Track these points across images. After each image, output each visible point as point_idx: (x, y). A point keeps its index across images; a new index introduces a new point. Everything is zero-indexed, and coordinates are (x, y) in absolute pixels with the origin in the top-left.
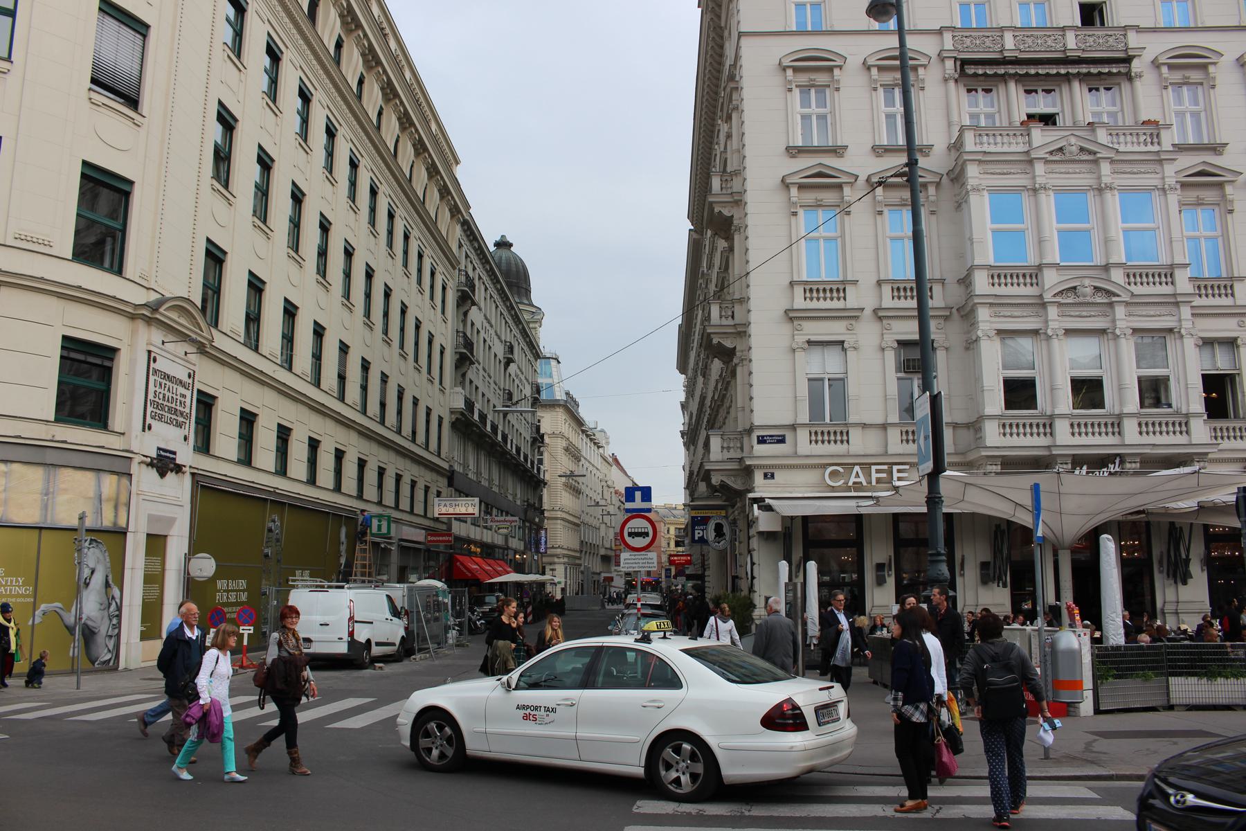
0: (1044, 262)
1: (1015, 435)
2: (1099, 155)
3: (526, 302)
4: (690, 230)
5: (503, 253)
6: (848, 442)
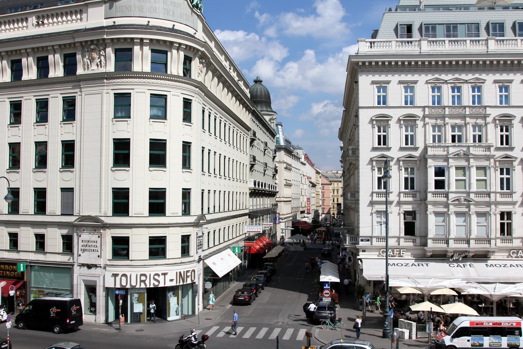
0: (450, 191)
1: (437, 244)
2: (470, 156)
3: (269, 110)
4: (344, 111)
5: (258, 86)
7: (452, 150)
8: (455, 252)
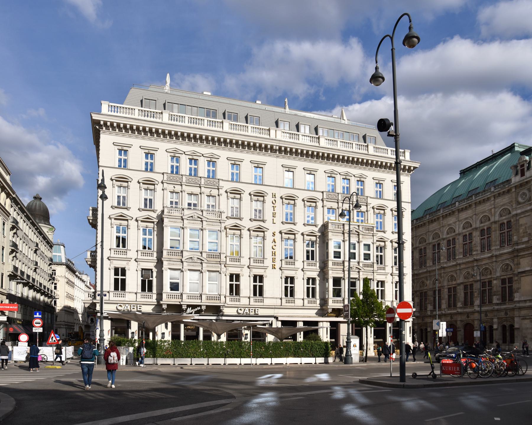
6: (294, 265)
7: (186, 212)
8: (188, 306)
